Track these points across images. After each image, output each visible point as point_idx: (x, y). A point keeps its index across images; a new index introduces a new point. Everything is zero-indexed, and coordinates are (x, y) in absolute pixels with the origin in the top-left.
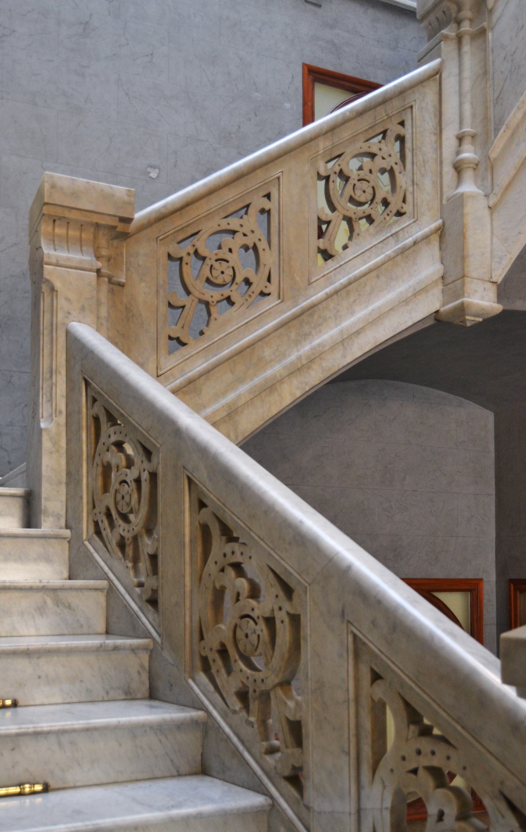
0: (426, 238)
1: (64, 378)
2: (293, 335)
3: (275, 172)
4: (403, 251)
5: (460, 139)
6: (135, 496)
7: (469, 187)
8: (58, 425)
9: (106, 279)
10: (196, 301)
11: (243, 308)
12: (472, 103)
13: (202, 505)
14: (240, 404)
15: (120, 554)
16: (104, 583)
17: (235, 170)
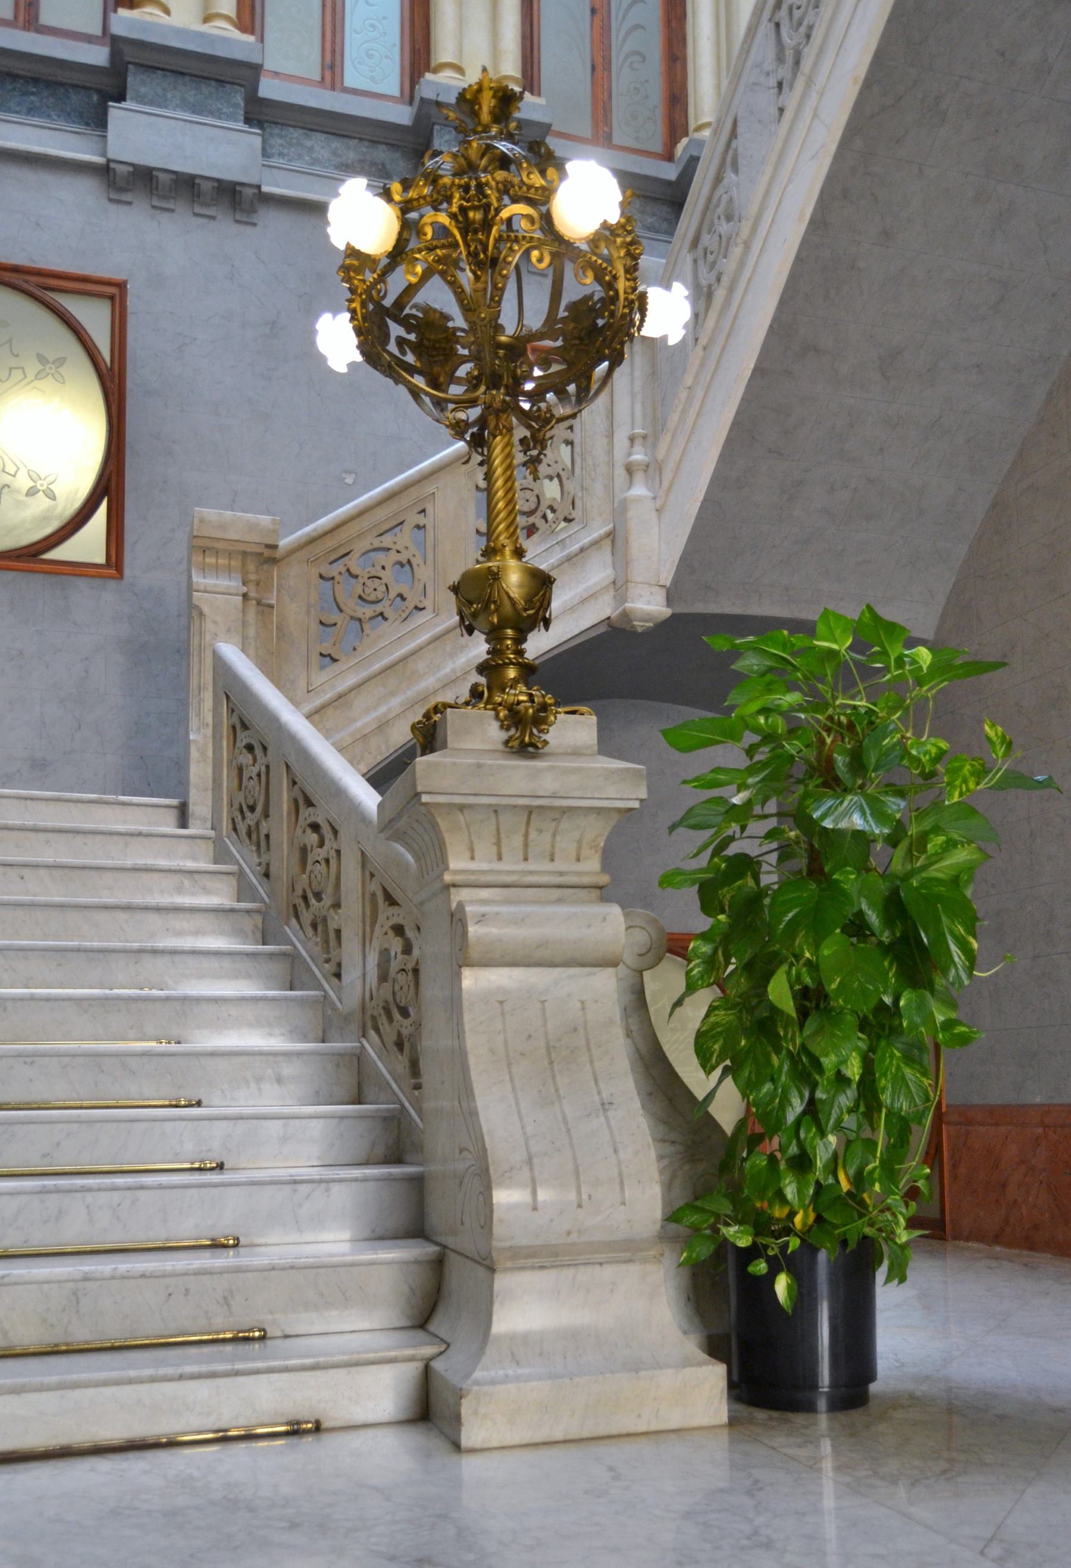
0: (596, 543)
1: (211, 694)
2: (448, 648)
3: (430, 488)
4: (569, 559)
5: (632, 439)
6: (257, 788)
7: (639, 490)
8: (205, 736)
9: (254, 602)
10: (348, 618)
11: (397, 622)
12: (643, 403)
13: (294, 783)
14: (391, 717)
15: (248, 841)
16: (233, 868)
17: (385, 490)
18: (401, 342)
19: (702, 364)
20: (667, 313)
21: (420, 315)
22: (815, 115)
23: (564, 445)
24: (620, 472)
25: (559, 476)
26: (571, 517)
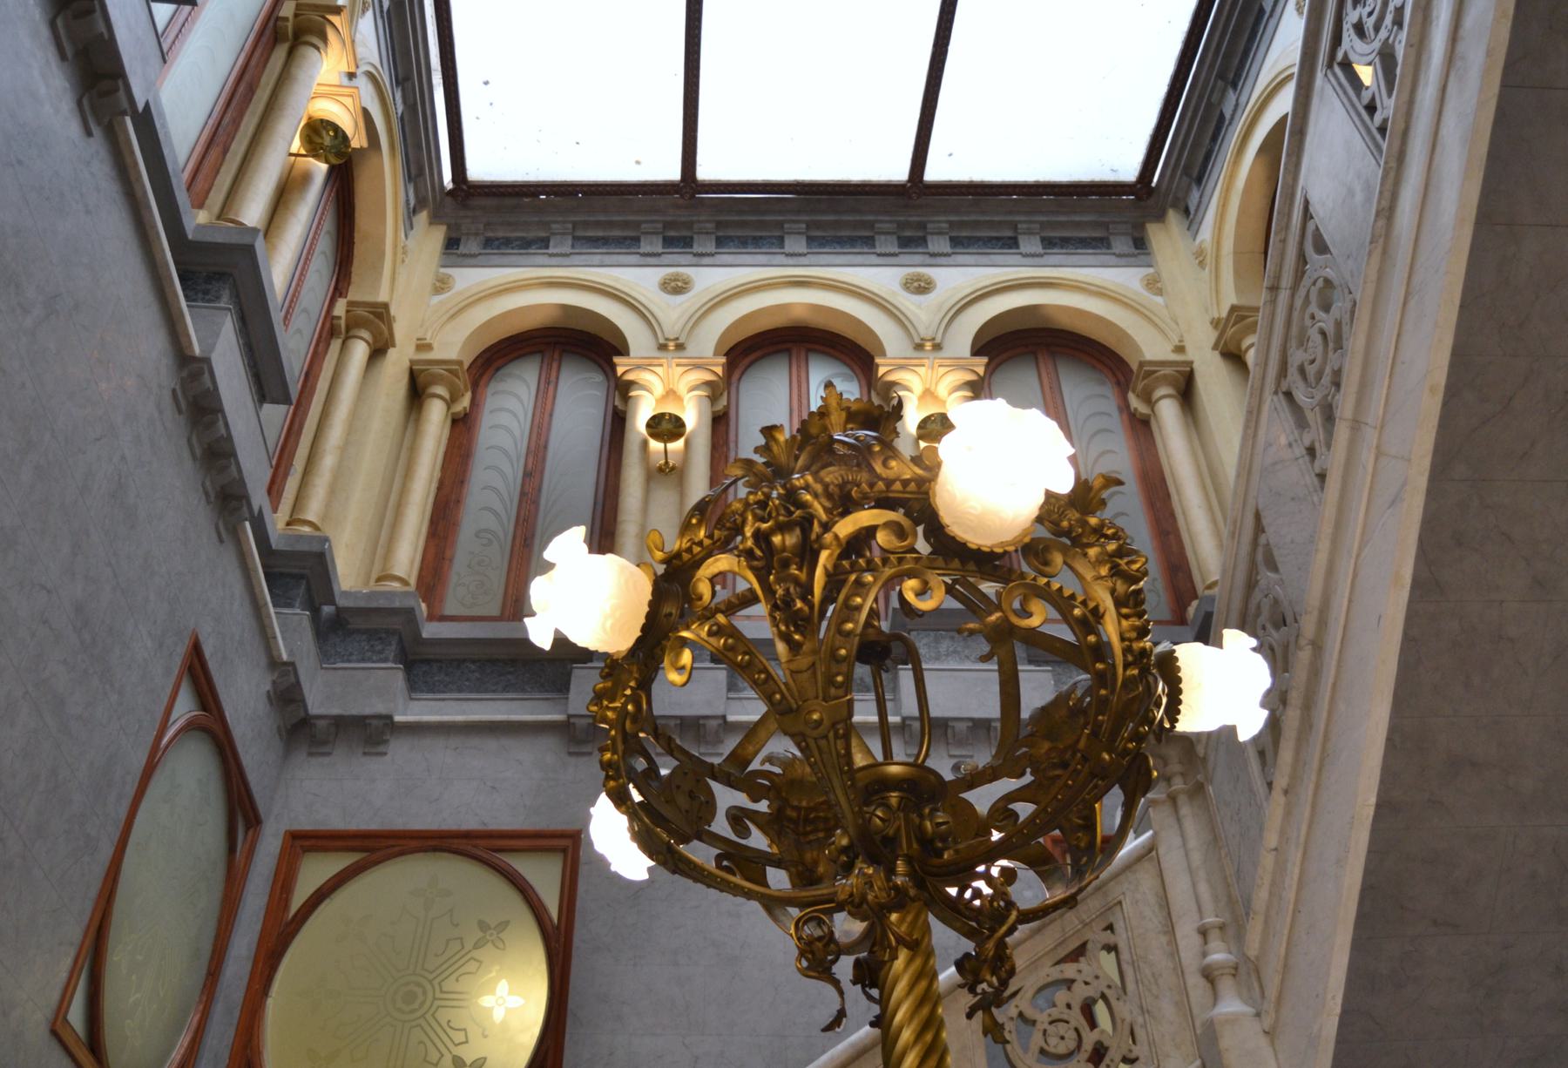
5: (1203, 933)
7: (1231, 1005)
17: (852, 1045)
18: (738, 817)
19: (1288, 814)
20: (1222, 687)
21: (778, 770)
22: (1379, 454)
23: (1104, 953)
24: (1195, 983)
25: (1103, 997)
26: (1132, 1056)
